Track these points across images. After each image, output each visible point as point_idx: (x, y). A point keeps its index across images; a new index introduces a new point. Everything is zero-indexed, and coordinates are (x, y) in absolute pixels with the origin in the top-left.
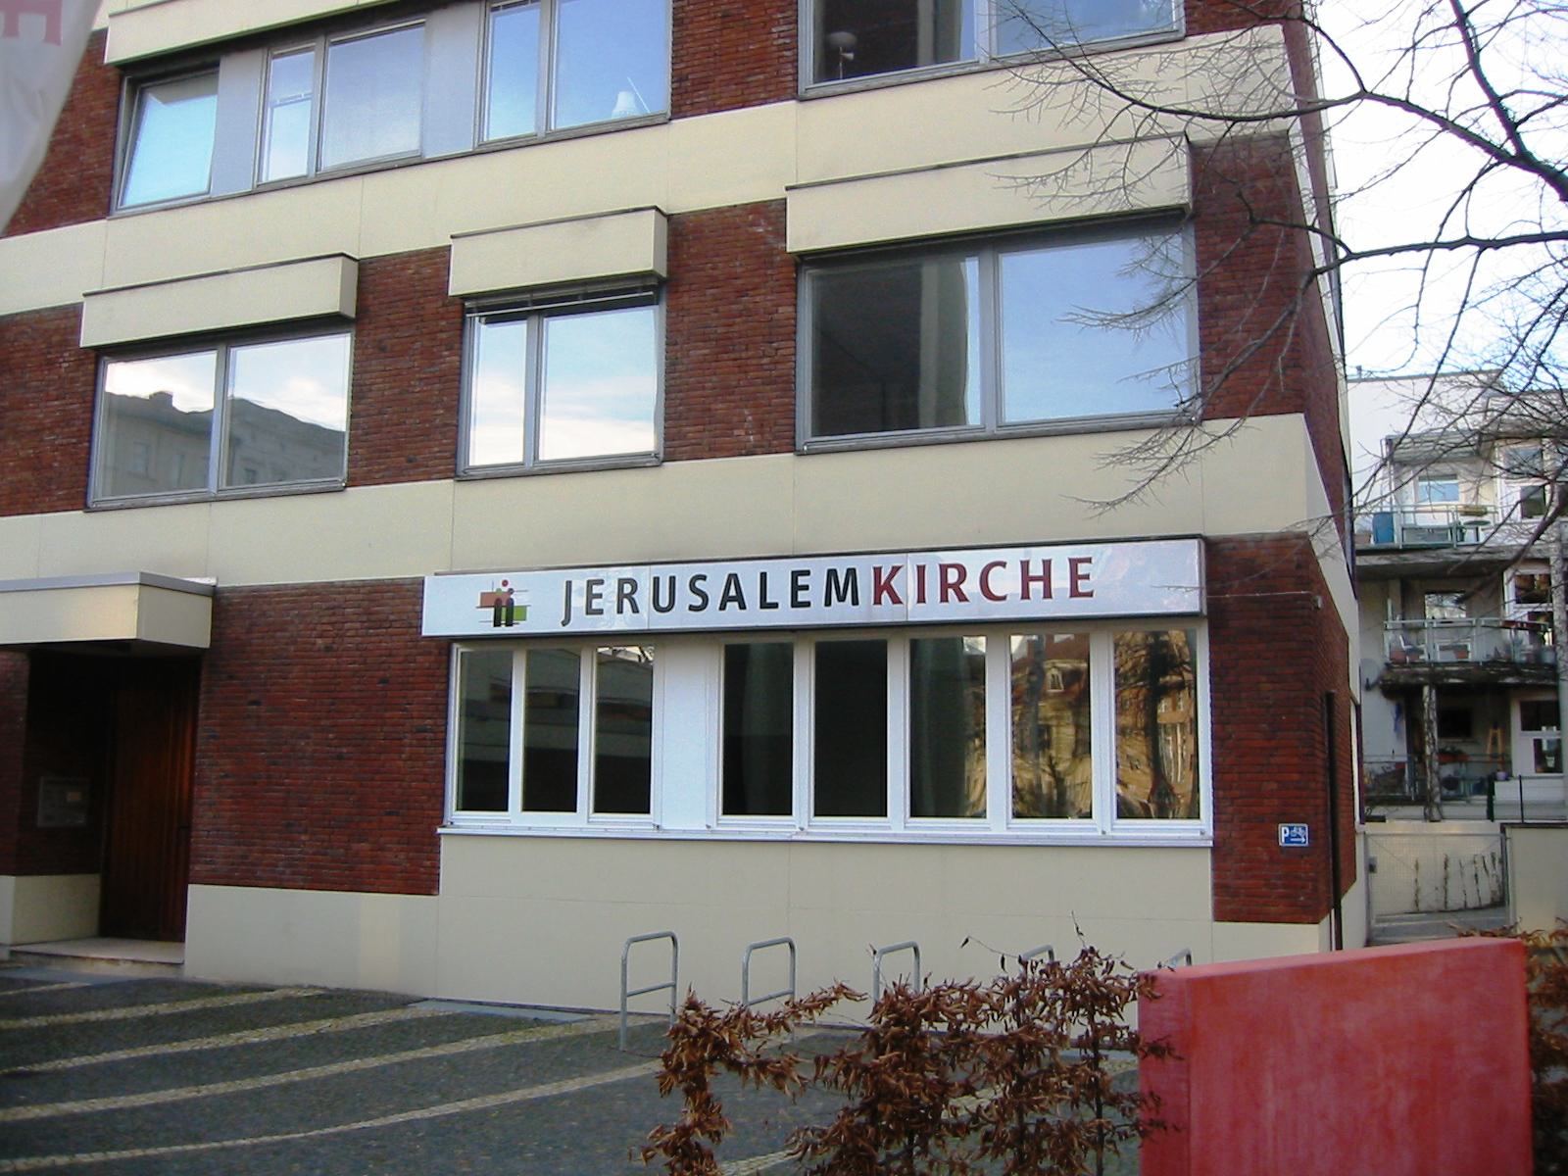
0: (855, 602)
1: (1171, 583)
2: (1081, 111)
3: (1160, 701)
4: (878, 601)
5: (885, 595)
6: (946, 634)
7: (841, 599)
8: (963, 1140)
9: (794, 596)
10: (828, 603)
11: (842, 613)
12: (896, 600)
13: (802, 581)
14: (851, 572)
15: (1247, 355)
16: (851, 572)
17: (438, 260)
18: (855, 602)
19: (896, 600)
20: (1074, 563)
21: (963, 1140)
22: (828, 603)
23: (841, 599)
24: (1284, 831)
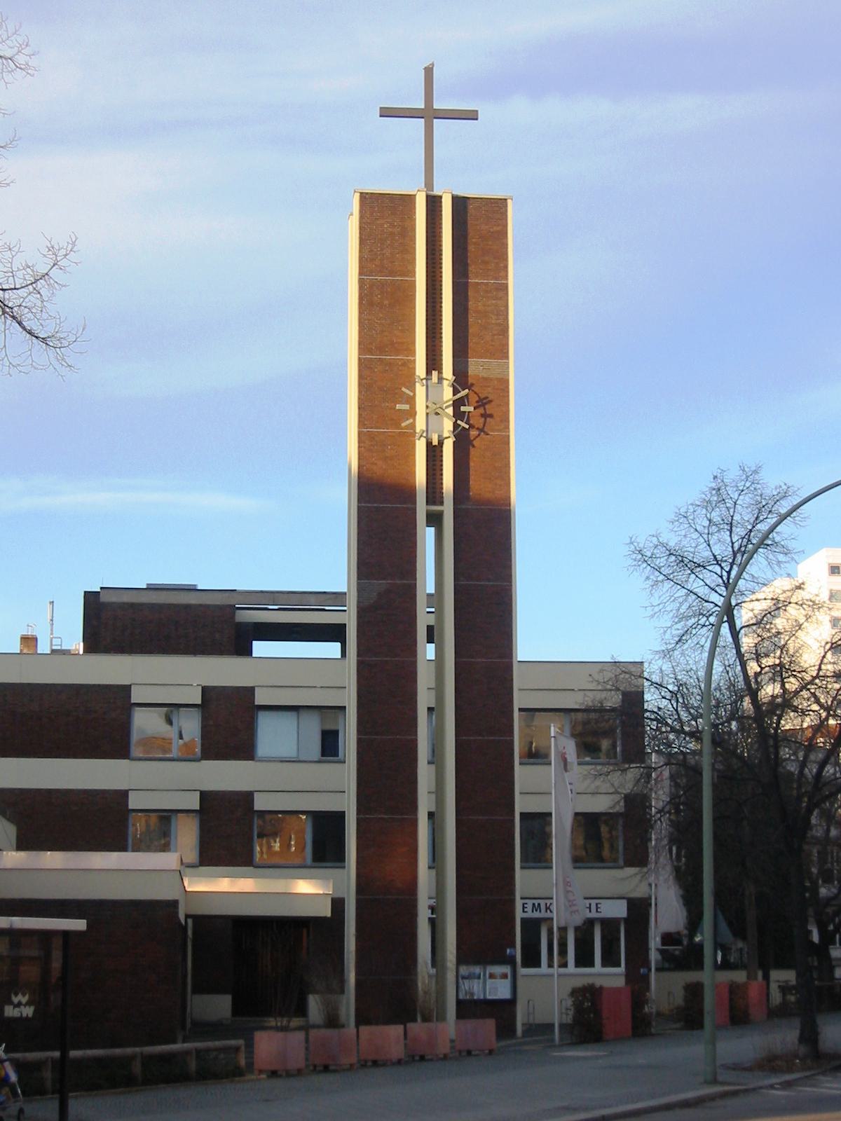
0: (540, 911)
1: (618, 910)
2: (709, 534)
3: (780, 1004)
4: (546, 911)
5: (548, 911)
6: (316, 864)
7: (536, 910)
8: (751, 475)
9: (523, 909)
10: (533, 911)
11: (536, 915)
12: (551, 911)
13: (525, 906)
14: (539, 904)
15: (771, 750)
16: (539, 904)
17: (251, 690)
18: (540, 911)
19: (551, 911)
20: (597, 904)
21: (751, 475)
22: (533, 911)
23: (536, 910)
24: (642, 970)
